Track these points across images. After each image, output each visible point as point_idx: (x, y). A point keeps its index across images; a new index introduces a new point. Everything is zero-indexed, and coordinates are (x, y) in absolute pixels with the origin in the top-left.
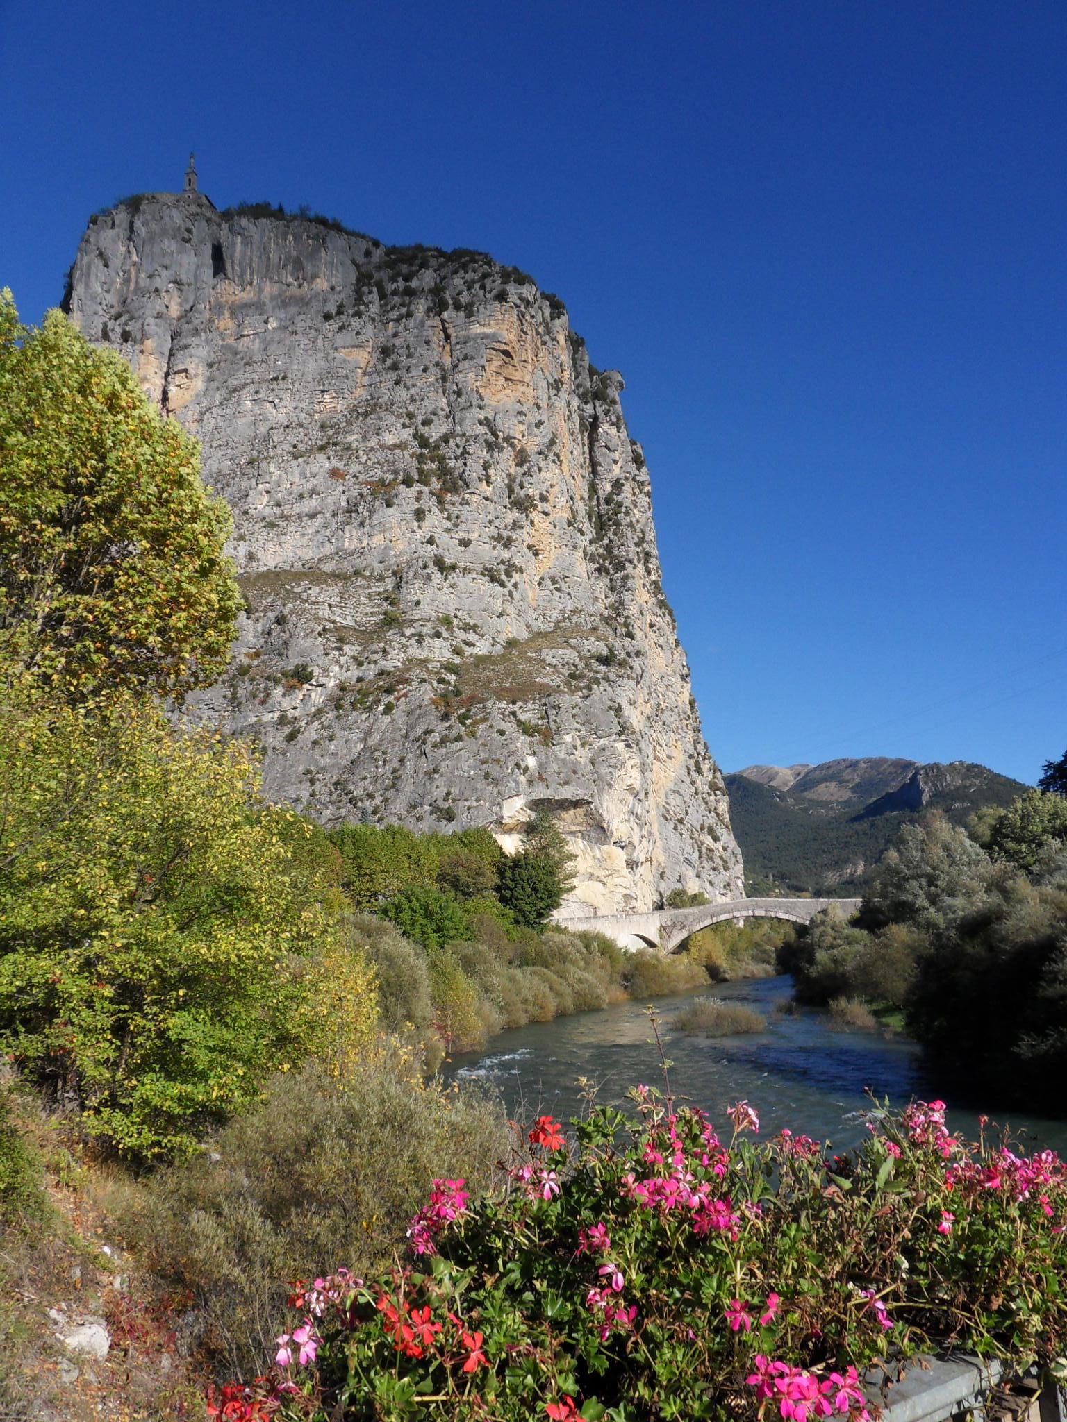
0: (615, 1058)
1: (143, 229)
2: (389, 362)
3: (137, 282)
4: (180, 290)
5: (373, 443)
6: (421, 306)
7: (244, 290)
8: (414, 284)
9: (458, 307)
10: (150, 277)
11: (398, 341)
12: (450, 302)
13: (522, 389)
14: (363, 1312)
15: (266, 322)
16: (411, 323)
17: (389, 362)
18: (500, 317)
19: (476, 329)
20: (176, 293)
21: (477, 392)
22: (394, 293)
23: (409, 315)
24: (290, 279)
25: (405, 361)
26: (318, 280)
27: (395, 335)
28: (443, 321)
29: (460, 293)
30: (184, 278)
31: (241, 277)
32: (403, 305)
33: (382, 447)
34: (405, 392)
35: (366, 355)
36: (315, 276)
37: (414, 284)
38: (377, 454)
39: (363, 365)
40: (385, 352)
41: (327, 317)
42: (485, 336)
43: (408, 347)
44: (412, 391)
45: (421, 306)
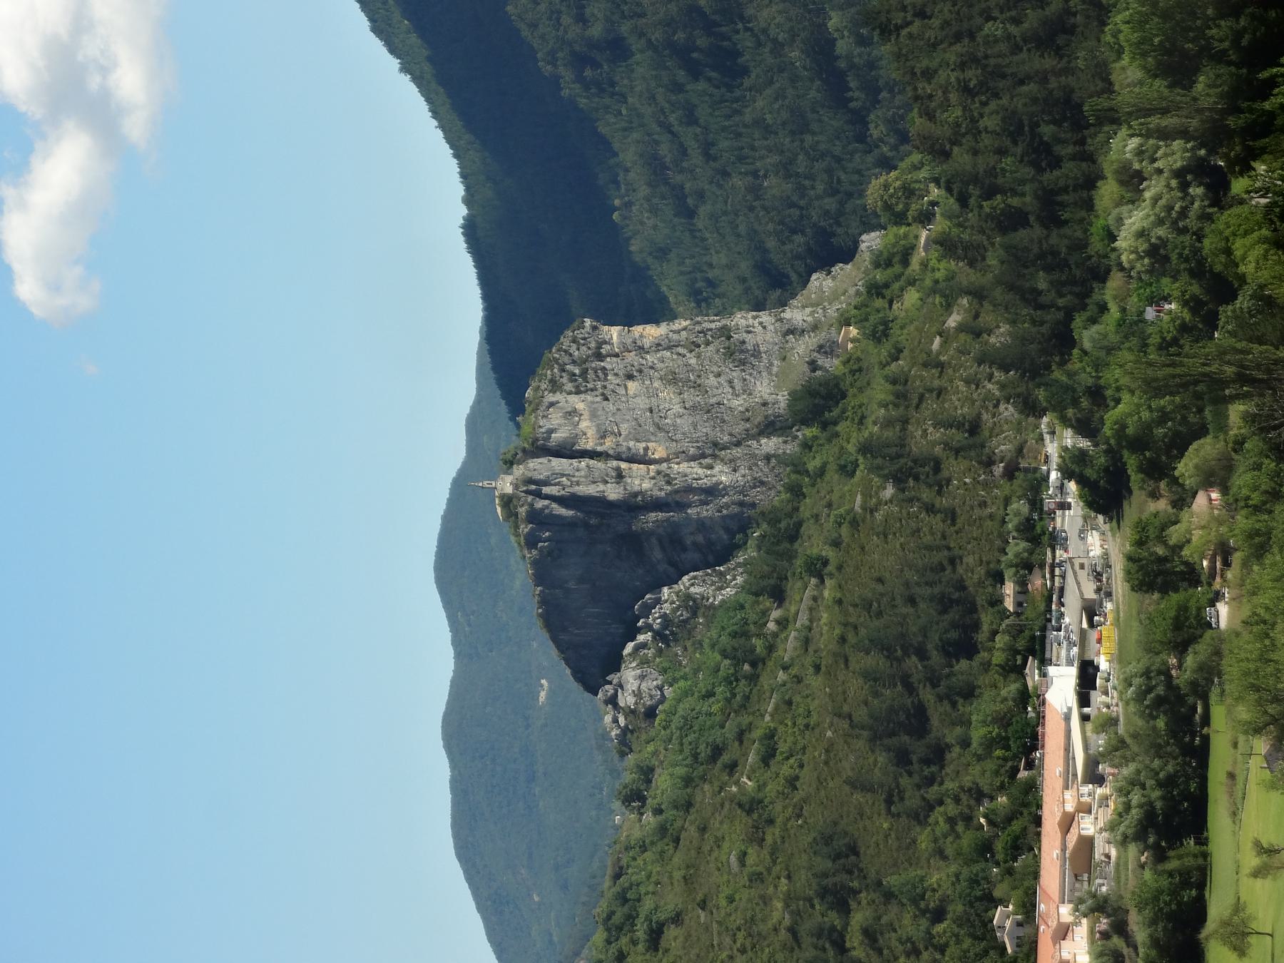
37: (577, 371)
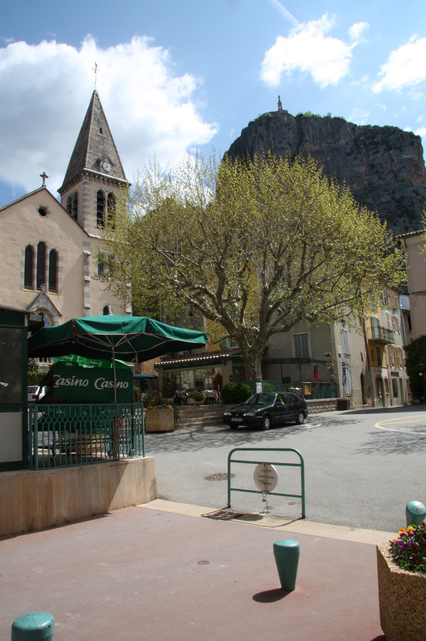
0: (77, 431)
1: (274, 125)
2: (374, 170)
3: (275, 145)
4: (291, 147)
5: (378, 202)
6: (381, 148)
7: (315, 146)
8: (376, 140)
9: (396, 148)
10: (280, 143)
11: (376, 162)
12: (393, 146)
13: (422, 178)
14: (362, 507)
15: (327, 158)
16: (379, 155)
17: (374, 170)
18: (412, 152)
19: (404, 156)
20: (290, 149)
21: (409, 181)
22: (369, 144)
23: (378, 152)
24: (331, 141)
25: (380, 170)
26: (341, 141)
27: (374, 160)
28: (390, 154)
29: (395, 143)
30: (291, 142)
31: (313, 141)
32: (374, 148)
33: (383, 203)
34: (383, 182)
35: (365, 168)
36: (340, 139)
38: (381, 206)
39: (364, 172)
40: (372, 166)
41: (348, 154)
42: (408, 159)
43: (380, 164)
44: (385, 181)
45: (381, 148)
